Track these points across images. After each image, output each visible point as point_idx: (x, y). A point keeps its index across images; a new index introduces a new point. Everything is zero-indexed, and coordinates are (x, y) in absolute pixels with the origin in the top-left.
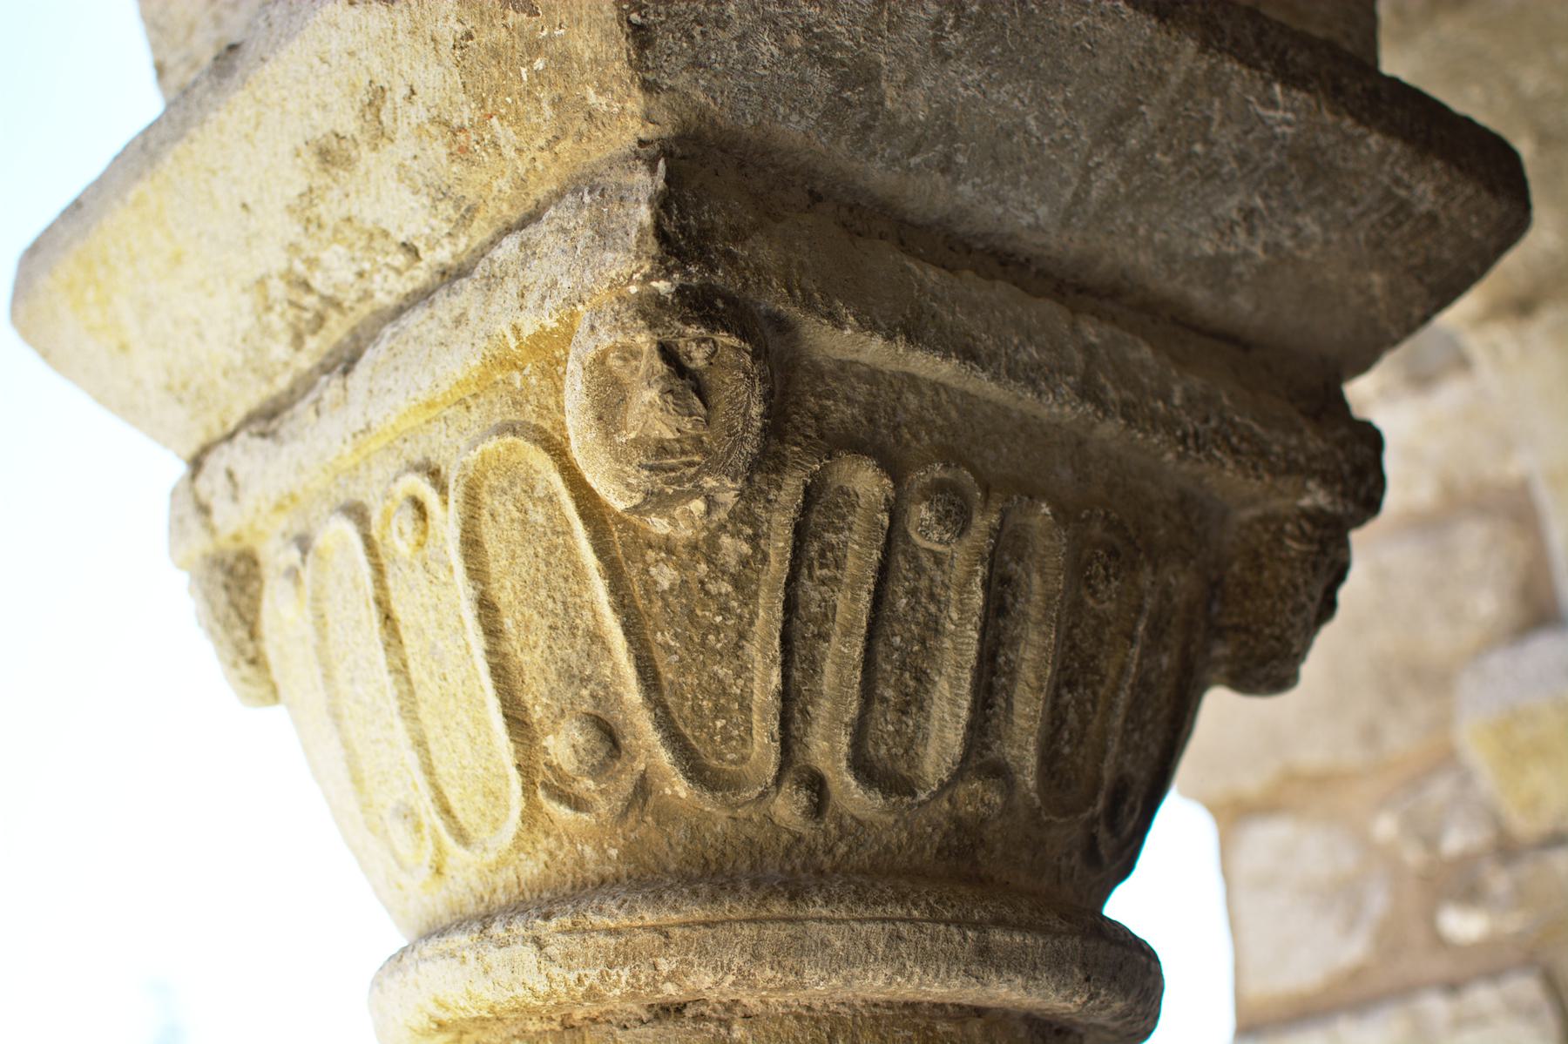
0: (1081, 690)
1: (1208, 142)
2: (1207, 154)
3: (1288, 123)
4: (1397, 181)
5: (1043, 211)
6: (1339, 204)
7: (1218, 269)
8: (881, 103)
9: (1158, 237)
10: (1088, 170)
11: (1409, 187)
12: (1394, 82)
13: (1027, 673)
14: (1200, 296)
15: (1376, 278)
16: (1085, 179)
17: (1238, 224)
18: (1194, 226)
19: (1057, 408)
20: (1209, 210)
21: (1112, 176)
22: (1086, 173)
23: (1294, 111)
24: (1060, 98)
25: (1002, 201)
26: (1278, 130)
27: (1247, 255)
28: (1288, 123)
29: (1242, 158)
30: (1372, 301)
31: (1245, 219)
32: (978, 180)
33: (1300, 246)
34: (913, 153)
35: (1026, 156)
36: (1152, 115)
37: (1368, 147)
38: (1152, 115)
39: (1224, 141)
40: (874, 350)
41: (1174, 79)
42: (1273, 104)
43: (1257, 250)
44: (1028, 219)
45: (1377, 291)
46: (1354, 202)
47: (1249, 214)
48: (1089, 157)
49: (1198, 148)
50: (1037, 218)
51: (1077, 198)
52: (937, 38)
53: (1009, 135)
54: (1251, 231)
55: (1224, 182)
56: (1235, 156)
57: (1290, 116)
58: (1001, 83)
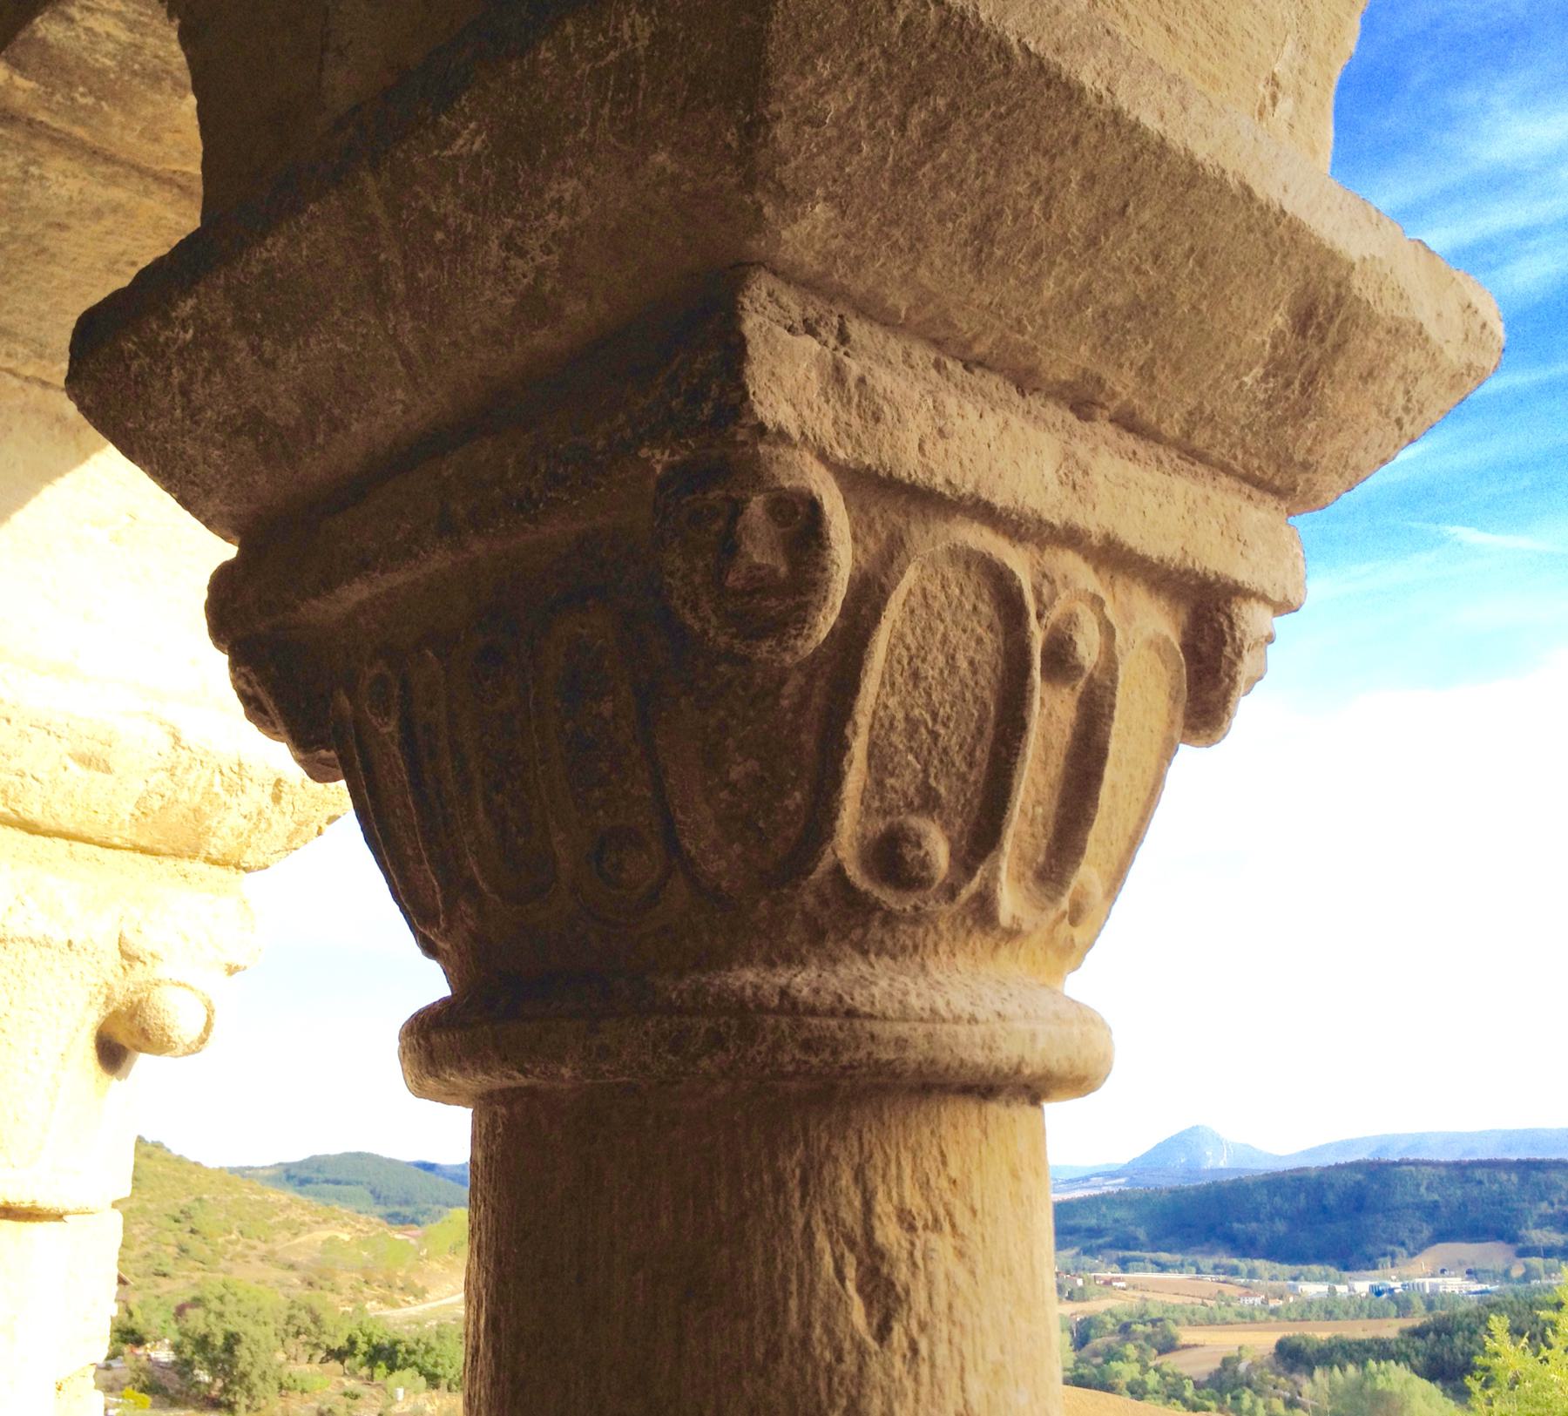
0: (509, 786)
1: (441, 223)
2: (448, 233)
3: (478, 132)
4: (597, 55)
5: (400, 394)
6: (569, 141)
7: (535, 307)
8: (277, 426)
9: (475, 329)
10: (394, 337)
11: (613, 45)
12: (203, 218)
13: (1552, 371)
14: (542, 338)
15: (661, 158)
16: (400, 346)
17: (508, 258)
18: (488, 294)
19: (439, 560)
20: (485, 272)
21: (409, 326)
22: (393, 338)
23: (470, 119)
24: (338, 313)
25: (376, 413)
26: (476, 147)
27: (541, 271)
28: (478, 132)
29: (470, 206)
30: (675, 180)
31: (508, 249)
32: (355, 415)
33: (574, 213)
34: (314, 437)
35: (360, 372)
36: (389, 255)
37: (546, 63)
38: (389, 255)
39: (450, 207)
40: (356, 593)
41: (379, 213)
42: (455, 135)
43: (541, 259)
44: (399, 408)
45: (672, 168)
46: (578, 124)
47: (508, 243)
48: (386, 331)
49: (439, 236)
50: (402, 402)
51: (407, 362)
52: (260, 357)
53: (341, 369)
54: (522, 253)
55: (476, 238)
56: (466, 209)
57: (472, 125)
58: (307, 344)
